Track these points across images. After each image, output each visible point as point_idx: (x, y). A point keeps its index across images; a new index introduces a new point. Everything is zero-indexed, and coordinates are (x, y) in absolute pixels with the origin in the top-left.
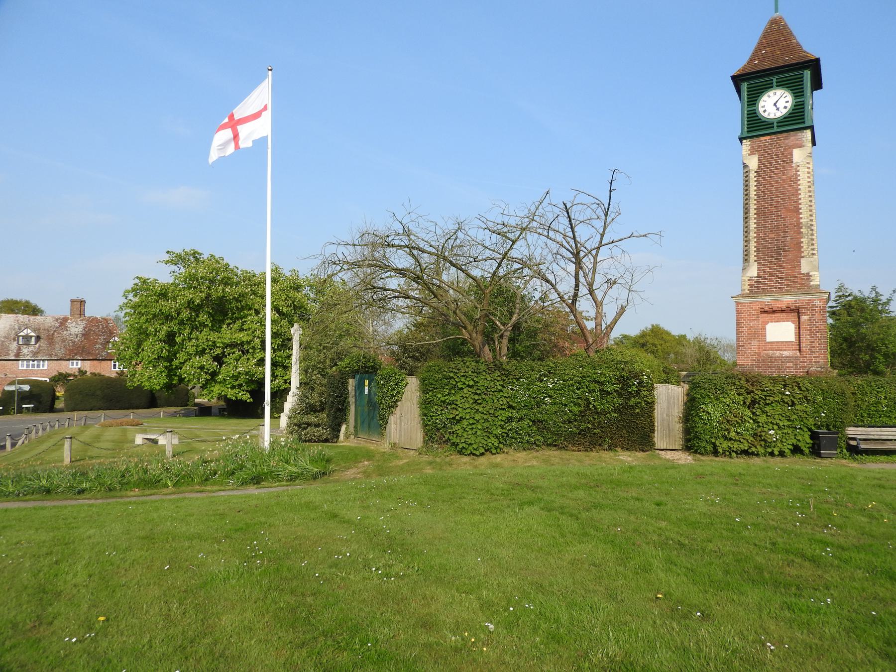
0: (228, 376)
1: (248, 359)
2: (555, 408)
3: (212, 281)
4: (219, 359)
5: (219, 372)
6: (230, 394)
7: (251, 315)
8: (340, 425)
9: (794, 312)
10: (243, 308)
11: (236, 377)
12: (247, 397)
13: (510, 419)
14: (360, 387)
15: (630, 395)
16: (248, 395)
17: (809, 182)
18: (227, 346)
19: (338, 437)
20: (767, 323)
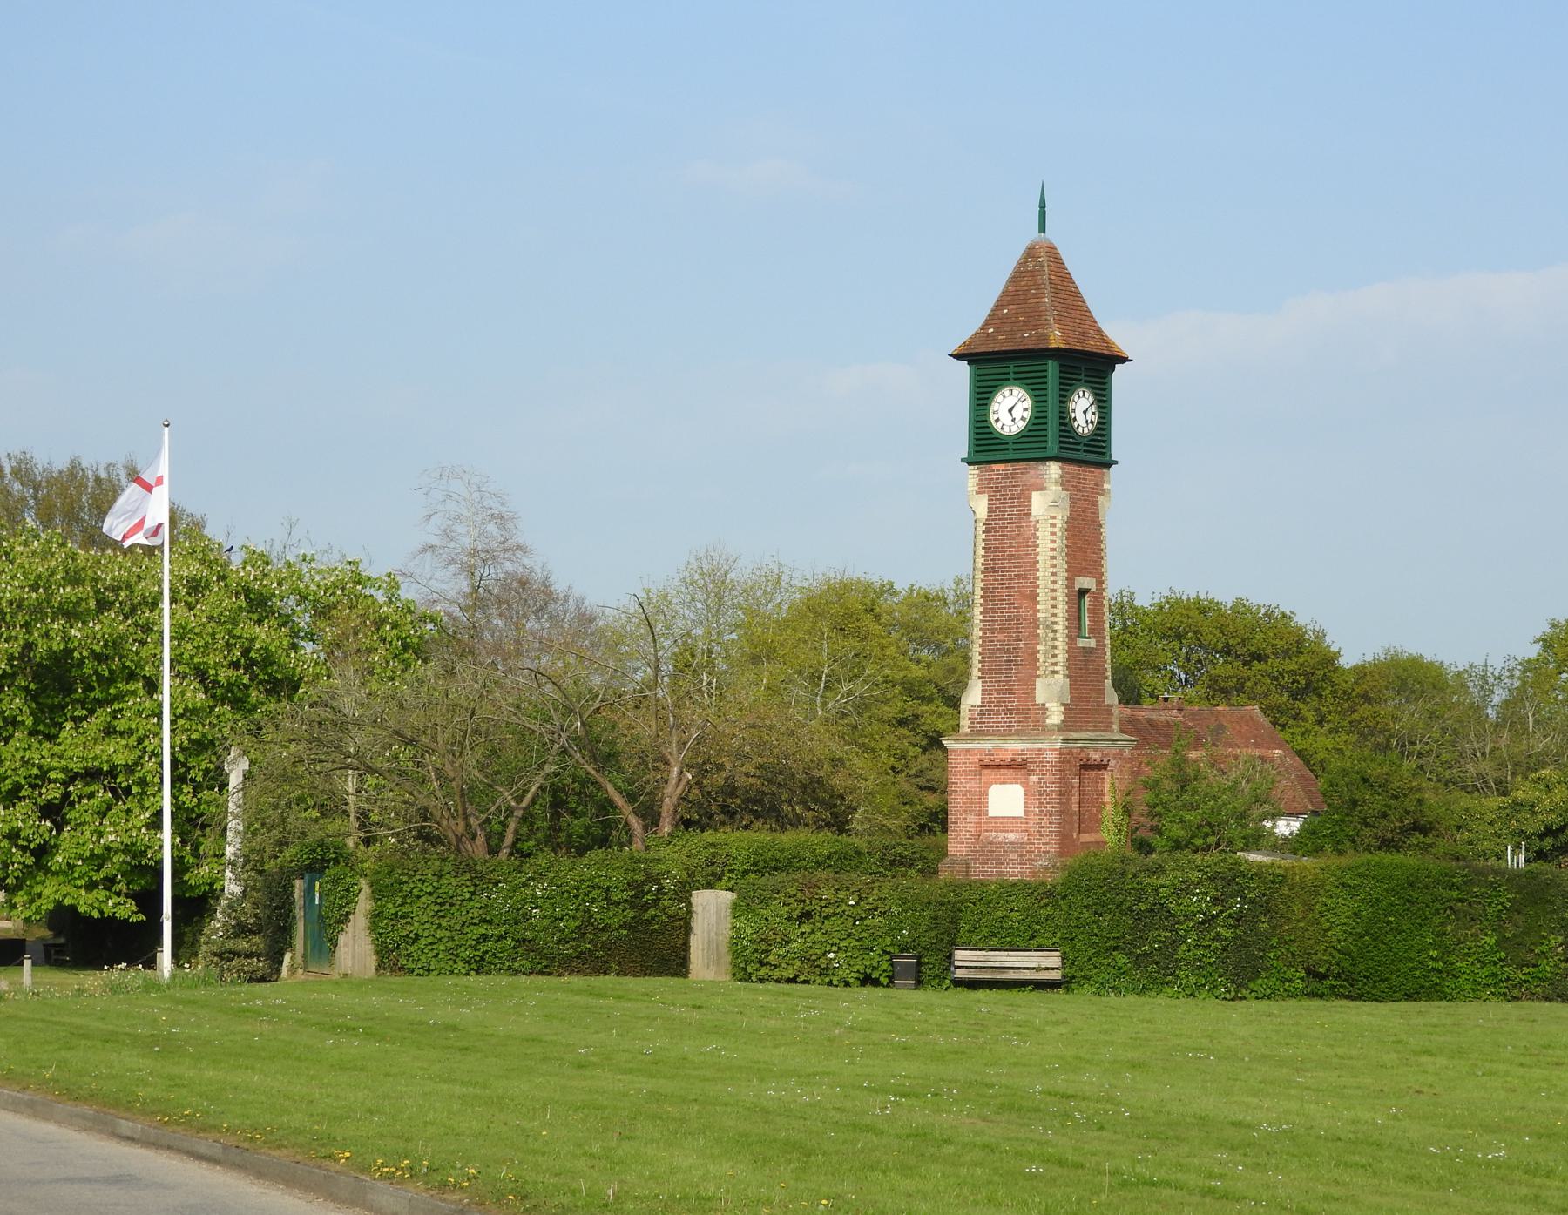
0: (80, 857)
1: (129, 811)
2: (546, 922)
3: (38, 612)
4: (53, 812)
5: (56, 846)
6: (86, 902)
7: (134, 693)
8: (283, 955)
9: (1017, 767)
10: (111, 680)
11: (98, 860)
12: (127, 910)
13: (485, 938)
14: (309, 891)
15: (646, 907)
16: (131, 906)
17: (1053, 550)
18: (73, 778)
19: (279, 972)
20: (988, 785)
